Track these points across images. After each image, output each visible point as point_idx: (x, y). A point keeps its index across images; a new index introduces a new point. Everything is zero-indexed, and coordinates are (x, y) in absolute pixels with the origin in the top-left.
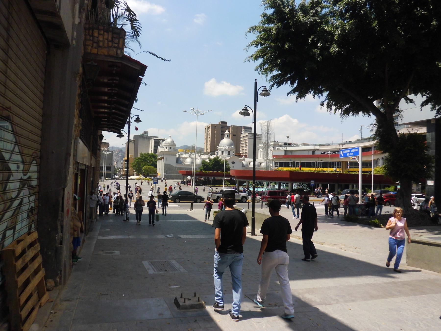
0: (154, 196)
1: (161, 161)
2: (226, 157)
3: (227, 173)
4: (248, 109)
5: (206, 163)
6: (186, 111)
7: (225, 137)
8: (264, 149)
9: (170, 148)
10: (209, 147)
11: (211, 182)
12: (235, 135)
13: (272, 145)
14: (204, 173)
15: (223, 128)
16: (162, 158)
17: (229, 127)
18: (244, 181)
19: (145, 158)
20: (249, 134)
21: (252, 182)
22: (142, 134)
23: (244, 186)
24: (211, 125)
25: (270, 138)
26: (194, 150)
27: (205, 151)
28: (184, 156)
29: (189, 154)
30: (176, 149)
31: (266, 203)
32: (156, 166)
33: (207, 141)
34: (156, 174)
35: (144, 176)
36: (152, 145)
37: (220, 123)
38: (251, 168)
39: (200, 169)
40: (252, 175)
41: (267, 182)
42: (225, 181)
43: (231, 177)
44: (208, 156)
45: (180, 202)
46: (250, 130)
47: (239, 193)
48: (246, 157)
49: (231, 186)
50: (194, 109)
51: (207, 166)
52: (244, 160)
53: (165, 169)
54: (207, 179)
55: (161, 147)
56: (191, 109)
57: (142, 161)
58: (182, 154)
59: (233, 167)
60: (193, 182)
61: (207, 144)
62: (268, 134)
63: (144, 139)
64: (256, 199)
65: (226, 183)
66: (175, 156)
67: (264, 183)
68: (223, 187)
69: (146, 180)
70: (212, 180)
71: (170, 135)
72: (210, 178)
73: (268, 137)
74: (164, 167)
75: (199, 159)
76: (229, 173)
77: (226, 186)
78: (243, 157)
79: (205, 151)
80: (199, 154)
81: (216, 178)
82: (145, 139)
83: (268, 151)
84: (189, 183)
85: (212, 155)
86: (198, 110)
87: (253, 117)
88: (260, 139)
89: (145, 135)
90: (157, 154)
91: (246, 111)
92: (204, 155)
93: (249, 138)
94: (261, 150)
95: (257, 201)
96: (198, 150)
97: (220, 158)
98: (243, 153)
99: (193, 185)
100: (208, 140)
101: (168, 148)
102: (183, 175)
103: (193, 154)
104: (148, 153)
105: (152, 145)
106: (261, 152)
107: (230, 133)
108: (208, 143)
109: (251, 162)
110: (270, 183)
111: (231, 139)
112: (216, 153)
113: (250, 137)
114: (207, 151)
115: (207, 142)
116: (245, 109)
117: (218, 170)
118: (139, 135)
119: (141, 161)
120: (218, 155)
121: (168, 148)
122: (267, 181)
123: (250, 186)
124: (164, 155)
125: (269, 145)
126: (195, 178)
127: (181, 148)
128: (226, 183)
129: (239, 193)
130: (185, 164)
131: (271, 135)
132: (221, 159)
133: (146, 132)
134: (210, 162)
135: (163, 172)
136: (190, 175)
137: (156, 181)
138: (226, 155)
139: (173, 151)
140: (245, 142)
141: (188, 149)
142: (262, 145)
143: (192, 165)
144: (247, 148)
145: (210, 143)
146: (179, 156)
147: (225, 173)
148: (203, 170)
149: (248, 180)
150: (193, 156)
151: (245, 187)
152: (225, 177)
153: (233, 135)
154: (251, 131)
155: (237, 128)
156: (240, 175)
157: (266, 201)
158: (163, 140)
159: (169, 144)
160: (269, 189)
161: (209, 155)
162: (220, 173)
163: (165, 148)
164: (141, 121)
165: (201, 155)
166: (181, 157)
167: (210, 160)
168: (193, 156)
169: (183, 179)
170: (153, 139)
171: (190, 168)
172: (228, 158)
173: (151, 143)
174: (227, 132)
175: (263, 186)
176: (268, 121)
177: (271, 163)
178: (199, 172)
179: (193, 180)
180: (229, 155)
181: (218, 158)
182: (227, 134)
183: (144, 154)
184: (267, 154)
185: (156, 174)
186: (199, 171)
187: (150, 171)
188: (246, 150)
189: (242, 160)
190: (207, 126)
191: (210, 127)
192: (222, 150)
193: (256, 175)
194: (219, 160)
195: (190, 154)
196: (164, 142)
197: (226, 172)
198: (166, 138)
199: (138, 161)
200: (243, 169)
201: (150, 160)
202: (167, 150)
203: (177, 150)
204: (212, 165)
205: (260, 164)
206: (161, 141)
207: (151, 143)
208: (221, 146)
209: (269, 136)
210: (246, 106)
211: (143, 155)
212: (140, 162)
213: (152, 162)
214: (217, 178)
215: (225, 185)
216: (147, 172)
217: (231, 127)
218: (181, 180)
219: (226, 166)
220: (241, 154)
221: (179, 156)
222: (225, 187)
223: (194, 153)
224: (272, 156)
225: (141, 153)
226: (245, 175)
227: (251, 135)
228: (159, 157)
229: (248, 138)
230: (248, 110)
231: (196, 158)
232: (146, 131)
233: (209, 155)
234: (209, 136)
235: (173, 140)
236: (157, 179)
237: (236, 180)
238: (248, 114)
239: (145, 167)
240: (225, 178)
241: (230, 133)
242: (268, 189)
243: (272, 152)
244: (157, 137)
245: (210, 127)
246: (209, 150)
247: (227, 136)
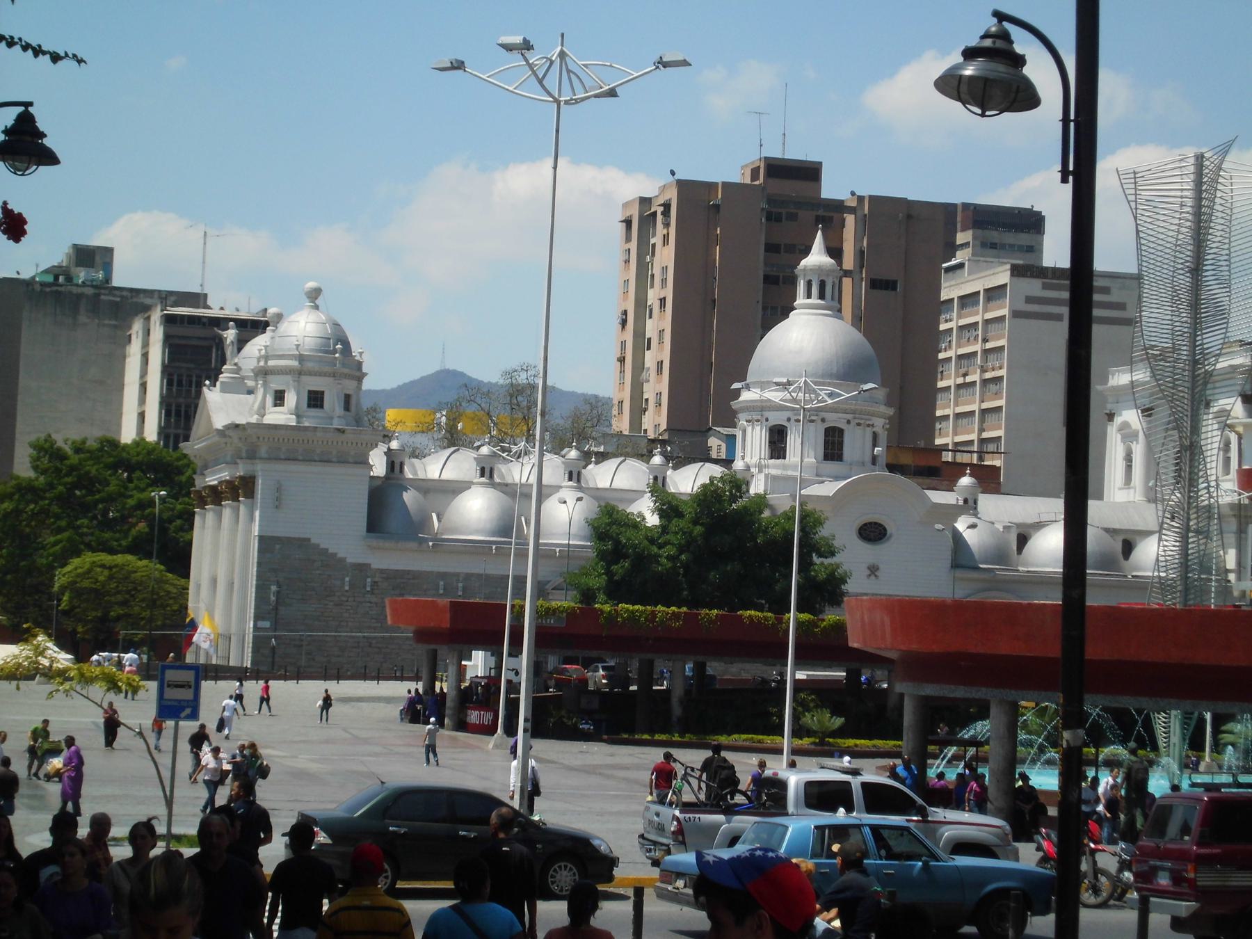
0: (161, 829)
1: (227, 513)
2: (805, 483)
3: (813, 624)
4: (1023, 43)
5: (630, 533)
6: (458, 66)
7: (800, 300)
8: (1163, 413)
9: (315, 400)
10: (657, 387)
11: (677, 711)
12: (889, 285)
13: (1240, 379)
14: (611, 618)
15: (778, 219)
16: (242, 488)
17: (838, 207)
18: (969, 702)
19: (76, 486)
20: (1016, 271)
21: (1042, 712)
22: (56, 271)
23: (974, 742)
24: (672, 195)
25: (1222, 314)
26: (528, 419)
27: (622, 425)
28: (435, 467)
29: (485, 450)
30: (366, 404)
31: (1185, 907)
32: (179, 560)
33: (640, 334)
34: (183, 626)
35: (65, 642)
36: (144, 372)
37: (755, 173)
38: (1040, 581)
39: (577, 587)
40: (1054, 650)
41: (1187, 716)
42: (795, 699)
43: (855, 659)
44: (652, 469)
45: (401, 884)
46: (1024, 239)
47: (922, 812)
48: (989, 480)
49: (851, 742)
50: (527, 46)
51: (642, 561)
52: (970, 506)
53: (261, 588)
54: (633, 675)
55: (225, 389)
56: (508, 48)
57: (55, 509)
58: (417, 454)
59: (873, 570)
60: (513, 706)
61: (639, 367)
62: (1196, 270)
63: (75, 310)
64: (1084, 867)
65: (808, 720)
66: (358, 470)
67: (1159, 721)
68: (779, 751)
69: (86, 680)
70: (678, 692)
71: (311, 284)
72: (662, 665)
73: (1195, 305)
74: (253, 570)
75: (570, 495)
76: (840, 628)
77: (806, 742)
78: (966, 481)
79: (622, 425)
80: (573, 454)
81: (714, 668)
82: (83, 318)
83: (1196, 429)
84: (474, 717)
85: (679, 462)
86: (562, 55)
87: (1065, 120)
88: (1128, 322)
89: (82, 275)
90: (194, 447)
91: (999, 69)
92: (612, 464)
93: (1016, 314)
94: (1131, 416)
95: (1096, 890)
96: (560, 417)
97: (757, 487)
98: (958, 447)
99: (511, 730)
100: (649, 393)
101: (291, 399)
102: (424, 635)
103: (519, 456)
104: (114, 444)
105: (144, 372)
106: (1128, 435)
107: (849, 262)
108: (650, 358)
109: (1039, 526)
110: (1219, 721)
111: (856, 321)
112: (716, 445)
113: (1030, 300)
114: (636, 422)
115: (642, 343)
116: (988, 43)
117: (733, 597)
118: (29, 283)
119: (45, 512)
120: (738, 465)
121: (291, 399)
122: (1188, 705)
123: (1029, 744)
124: (252, 455)
125: (1209, 374)
126: (537, 668)
127: (406, 395)
128: (808, 720)
129: (922, 812)
130: (441, 546)
131: (1226, 284)
132: (761, 501)
133: (87, 256)
134: (664, 529)
135: (243, 611)
136: (491, 641)
137: (187, 694)
138: (810, 460)
139: (336, 424)
140: (977, 347)
141: (470, 409)
142: (1142, 375)
143: (502, 551)
144: (1001, 402)
145: (664, 387)
146: (394, 465)
147: (799, 624)
148: (601, 597)
149: (1011, 694)
150: (520, 472)
151: (985, 760)
152: (801, 662)
153: (875, 284)
154: (1035, 249)
155: (909, 217)
156: (936, 649)
157: (1185, 889)
158: (251, 327)
159: (301, 358)
160: (1206, 779)
161: (657, 460)
162: (754, 624)
163: (270, 400)
164: (49, 158)
165: (586, 457)
166: (408, 474)
167: (669, 507)
168: (520, 472)
169: (425, 673)
170: (156, 316)
171: (487, 579)
172: (829, 489)
173: (135, 349)
174: (817, 257)
175: (1155, 748)
176: (1200, 158)
177: (1231, 538)
178: (571, 614)
179: (513, 687)
180: (832, 466)
181: (738, 485)
182: (819, 270)
183: (67, 449)
184: (1190, 452)
185: (183, 626)
186: (565, 601)
187: (124, 603)
188: (990, 419)
189: (952, 512)
190: (645, 201)
191: (667, 206)
192: (777, 418)
193: (1094, 651)
194: (745, 510)
195: (494, 455)
196: (258, 344)
197: (805, 616)
198: (272, 311)
199: (17, 512)
200: (960, 594)
201: (131, 502)
202: (279, 417)
203: (375, 413)
204: (681, 550)
205: (1118, 547)
206: (230, 334)
207: (134, 350)
208: (763, 385)
209: (1211, 287)
210: (1000, 16)
211: (58, 455)
212: (34, 515)
213: (150, 520)
214: (723, 670)
215: (798, 732)
216: (92, 615)
217: (852, 210)
218: (402, 689)
219: (812, 564)
220: (948, 457)
221: (391, 466)
222: (795, 752)
223: (530, 437)
224: (1233, 474)
225: (38, 435)
226: (981, 650)
227: (1034, 287)
228: (212, 480)
229: (1004, 312)
230: (1019, 61)
231: (544, 492)
232: (97, 240)
233: (657, 460)
234: (661, 291)
235: (336, 325)
236: (189, 676)
237: (899, 687)
238: (1024, 98)
239: (76, 562)
240: (801, 675)
241: (849, 262)
242: (1198, 779)
243: (1233, 438)
244: (197, 299)
245: (667, 206)
246: (655, 421)
247: (815, 290)
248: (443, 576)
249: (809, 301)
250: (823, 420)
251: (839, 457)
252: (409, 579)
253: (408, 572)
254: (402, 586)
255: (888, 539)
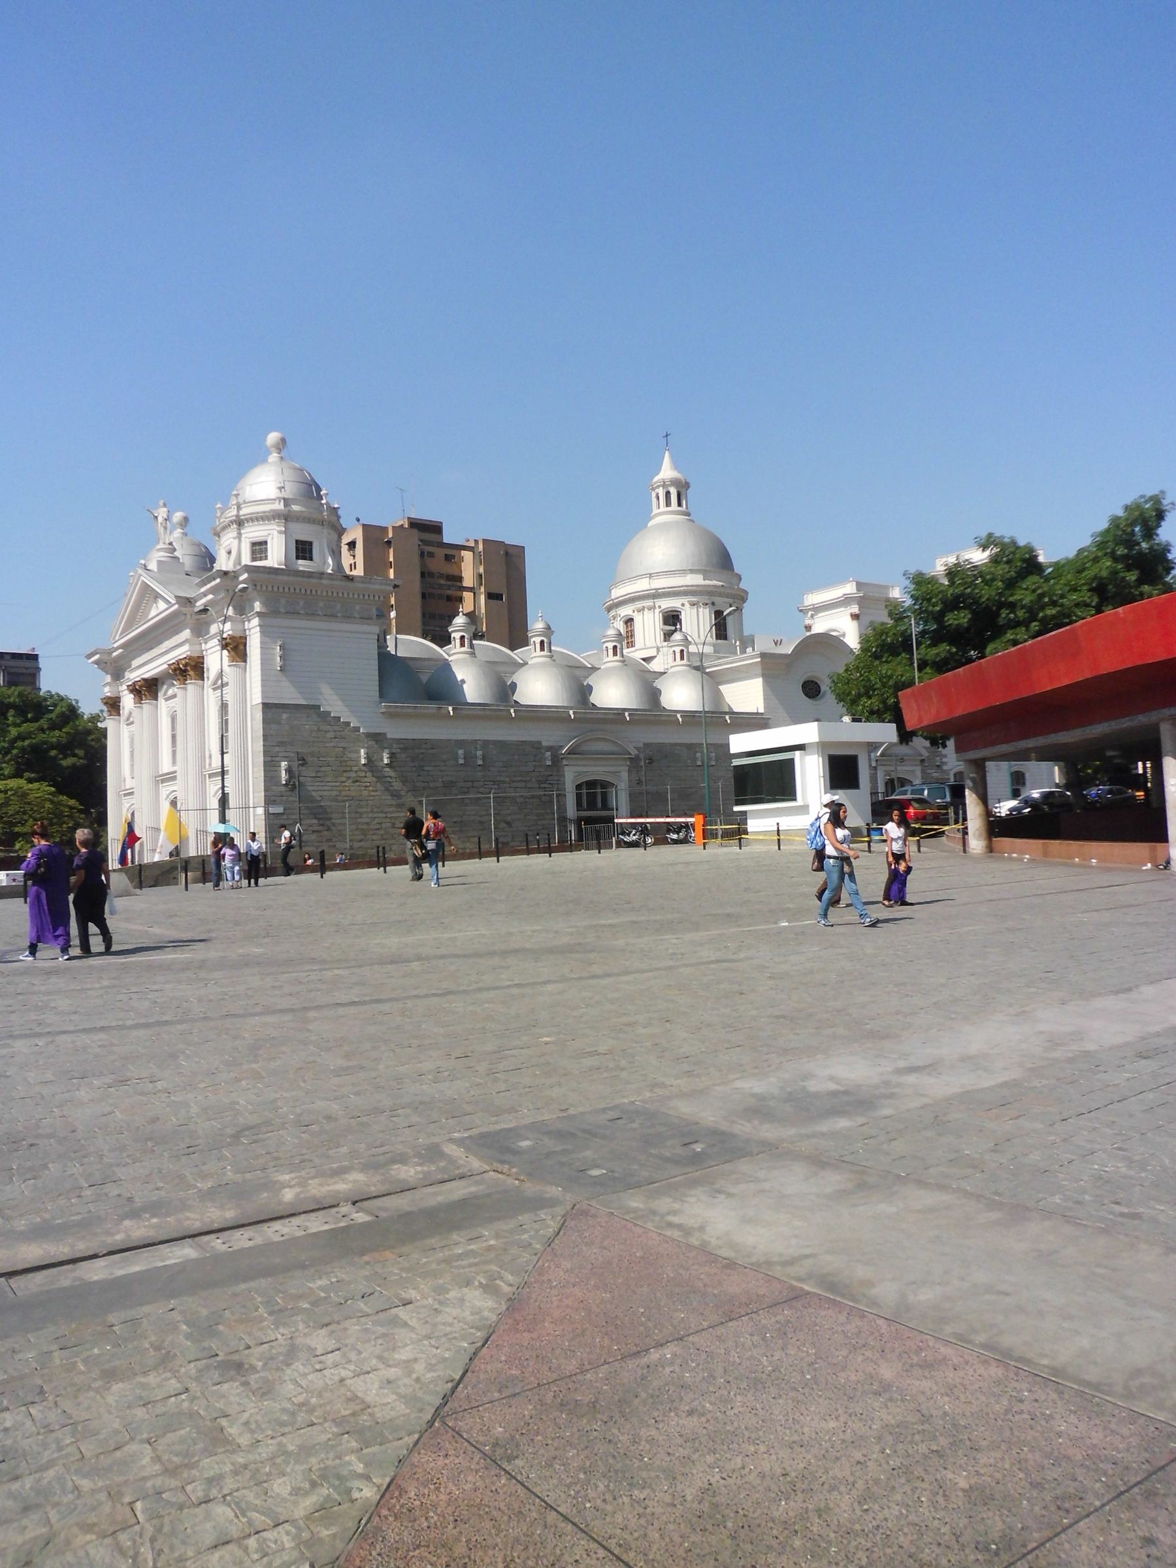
1: (190, 688)
53: (270, 766)
248: (461, 743)
249: (669, 509)
250: (713, 604)
251: (725, 638)
252: (427, 749)
253: (426, 741)
254: (421, 757)
255: (823, 696)
